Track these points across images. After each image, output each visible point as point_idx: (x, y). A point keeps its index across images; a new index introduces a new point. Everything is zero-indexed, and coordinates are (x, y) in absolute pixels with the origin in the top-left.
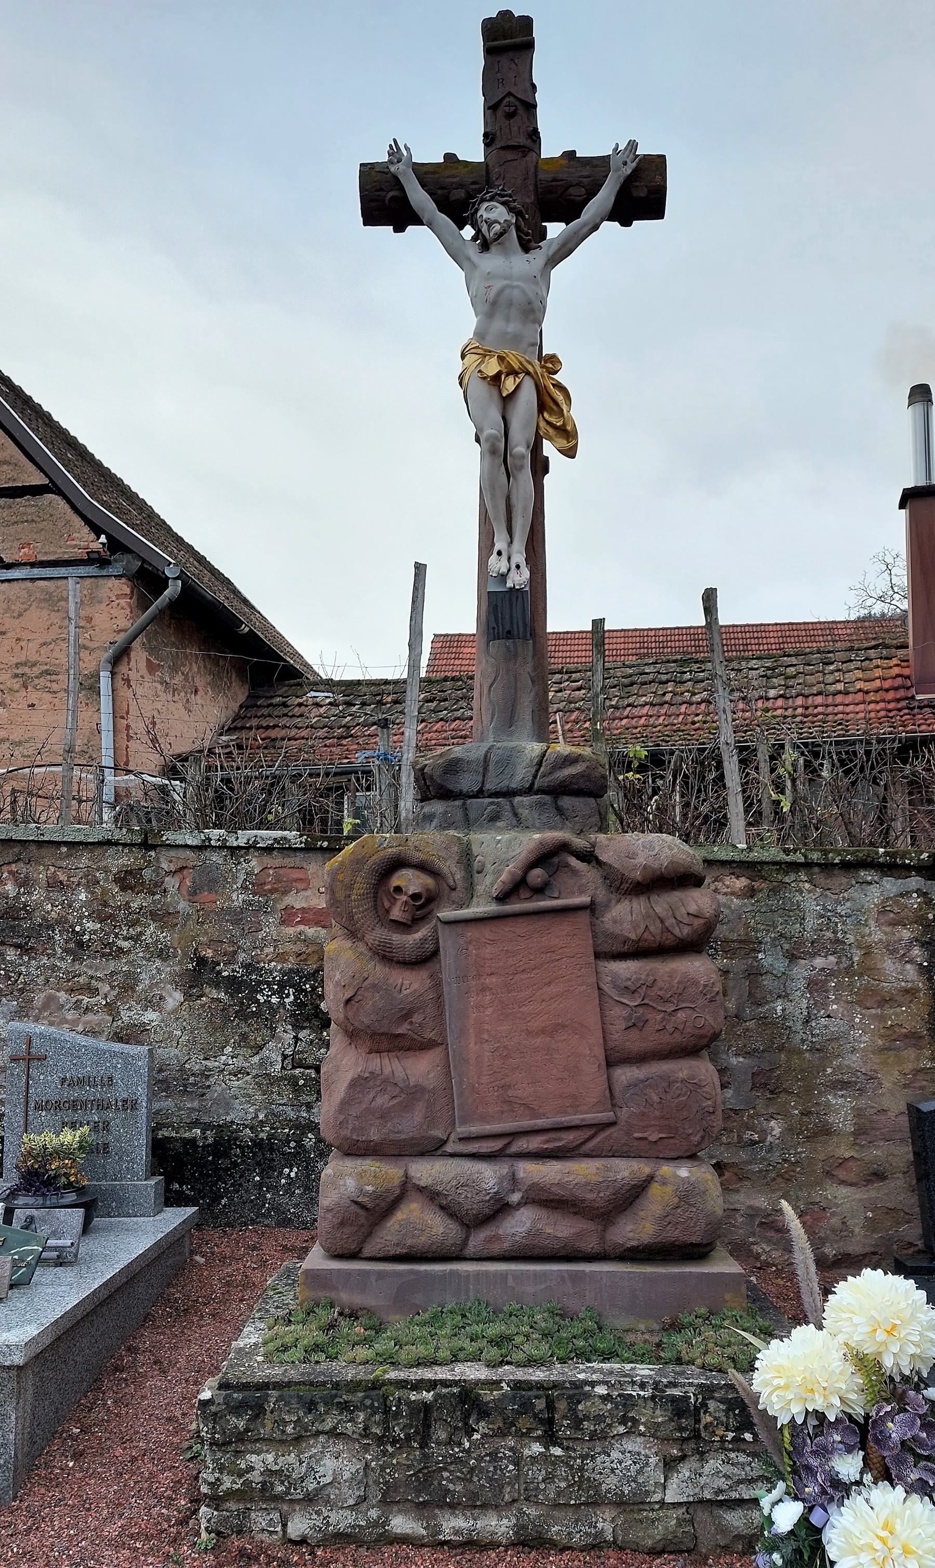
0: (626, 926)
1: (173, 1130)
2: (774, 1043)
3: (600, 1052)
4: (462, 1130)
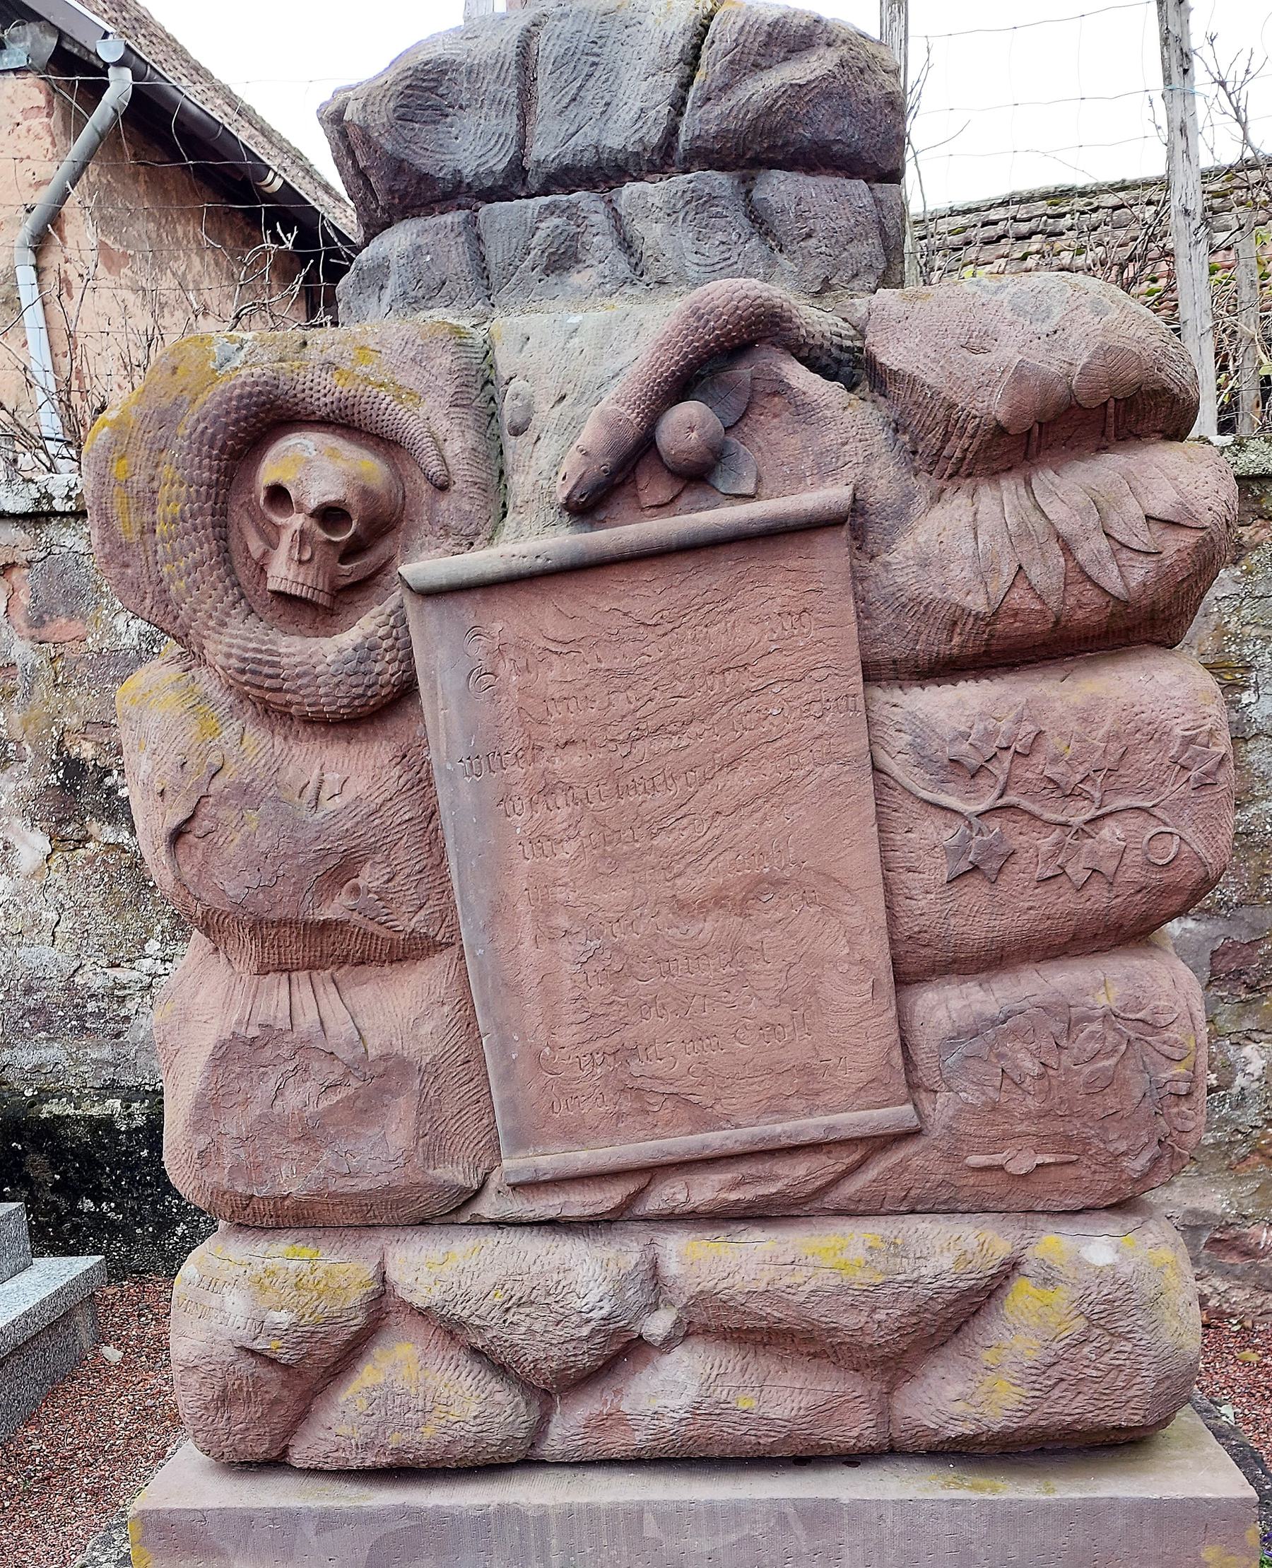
0: (960, 572)
1: (69, 1102)
2: (1263, 887)
3: (878, 952)
4: (515, 1164)
